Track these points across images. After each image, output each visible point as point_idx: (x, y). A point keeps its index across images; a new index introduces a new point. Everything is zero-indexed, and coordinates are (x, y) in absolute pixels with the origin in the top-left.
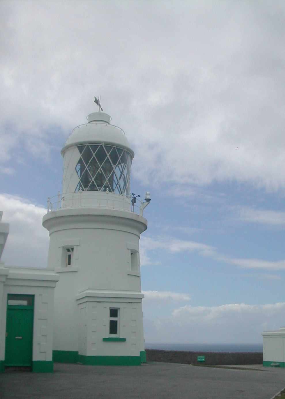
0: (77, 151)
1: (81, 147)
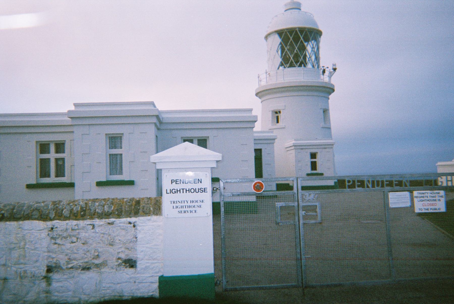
0: (277, 36)
1: (280, 33)
